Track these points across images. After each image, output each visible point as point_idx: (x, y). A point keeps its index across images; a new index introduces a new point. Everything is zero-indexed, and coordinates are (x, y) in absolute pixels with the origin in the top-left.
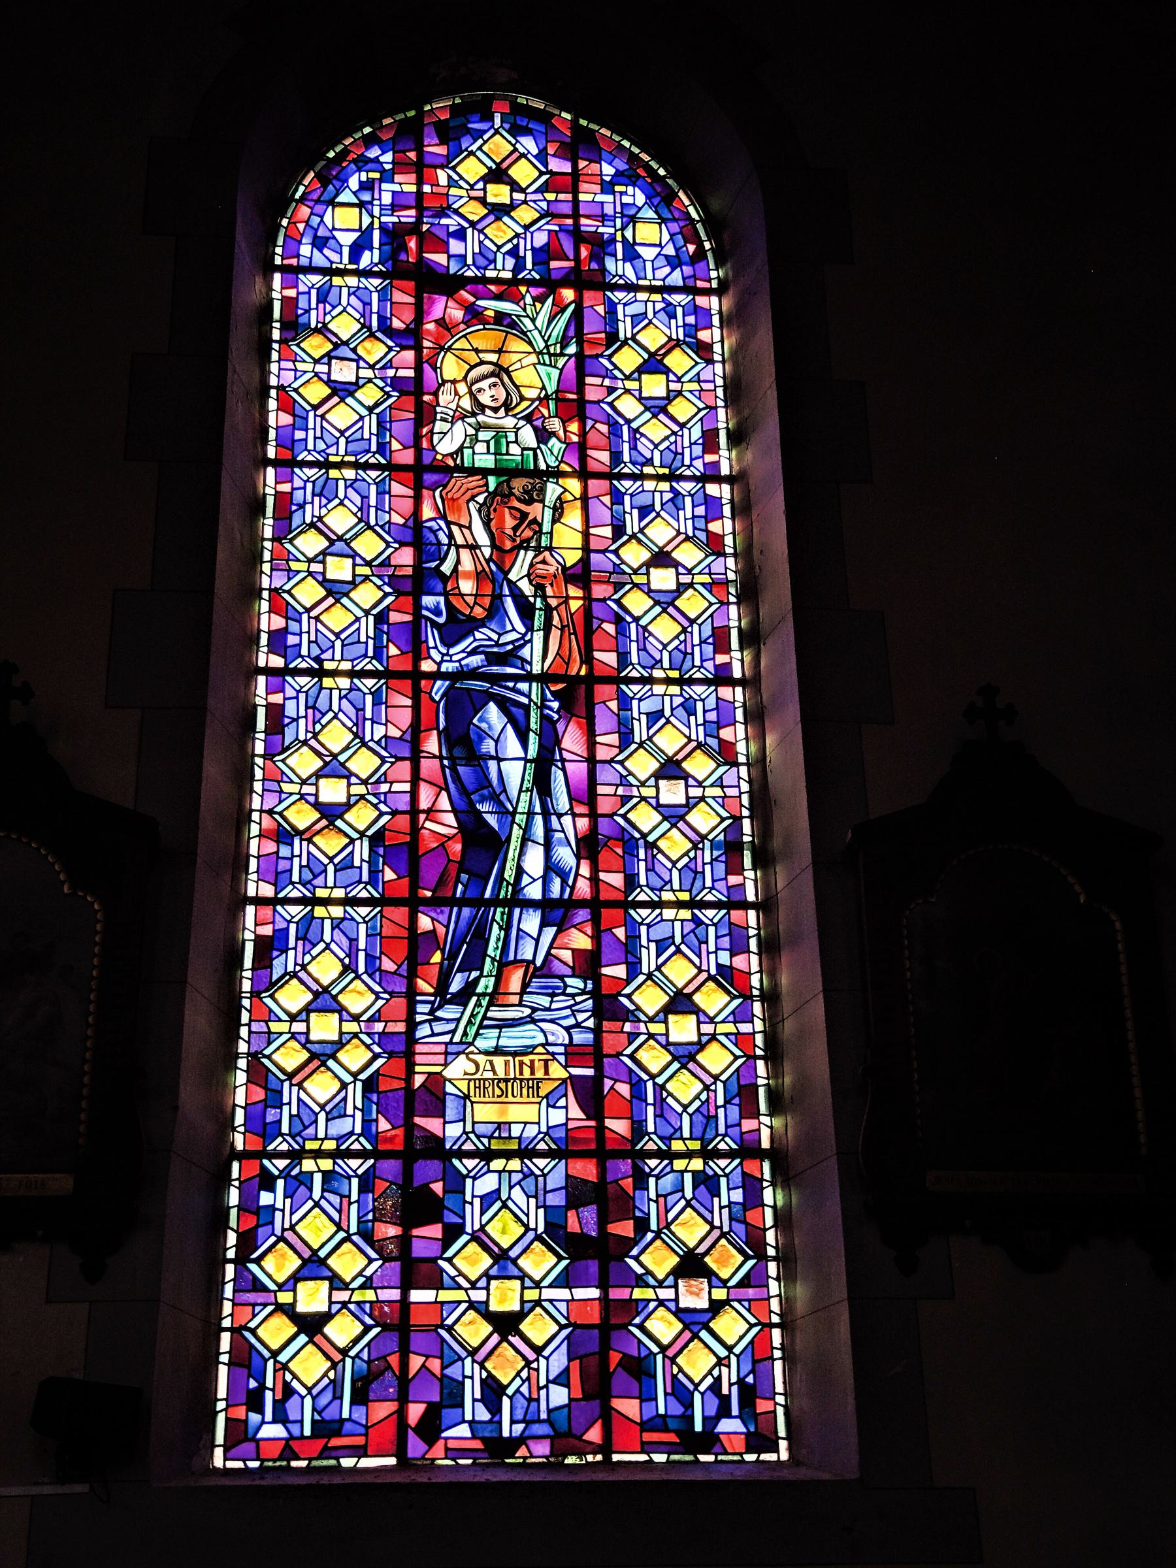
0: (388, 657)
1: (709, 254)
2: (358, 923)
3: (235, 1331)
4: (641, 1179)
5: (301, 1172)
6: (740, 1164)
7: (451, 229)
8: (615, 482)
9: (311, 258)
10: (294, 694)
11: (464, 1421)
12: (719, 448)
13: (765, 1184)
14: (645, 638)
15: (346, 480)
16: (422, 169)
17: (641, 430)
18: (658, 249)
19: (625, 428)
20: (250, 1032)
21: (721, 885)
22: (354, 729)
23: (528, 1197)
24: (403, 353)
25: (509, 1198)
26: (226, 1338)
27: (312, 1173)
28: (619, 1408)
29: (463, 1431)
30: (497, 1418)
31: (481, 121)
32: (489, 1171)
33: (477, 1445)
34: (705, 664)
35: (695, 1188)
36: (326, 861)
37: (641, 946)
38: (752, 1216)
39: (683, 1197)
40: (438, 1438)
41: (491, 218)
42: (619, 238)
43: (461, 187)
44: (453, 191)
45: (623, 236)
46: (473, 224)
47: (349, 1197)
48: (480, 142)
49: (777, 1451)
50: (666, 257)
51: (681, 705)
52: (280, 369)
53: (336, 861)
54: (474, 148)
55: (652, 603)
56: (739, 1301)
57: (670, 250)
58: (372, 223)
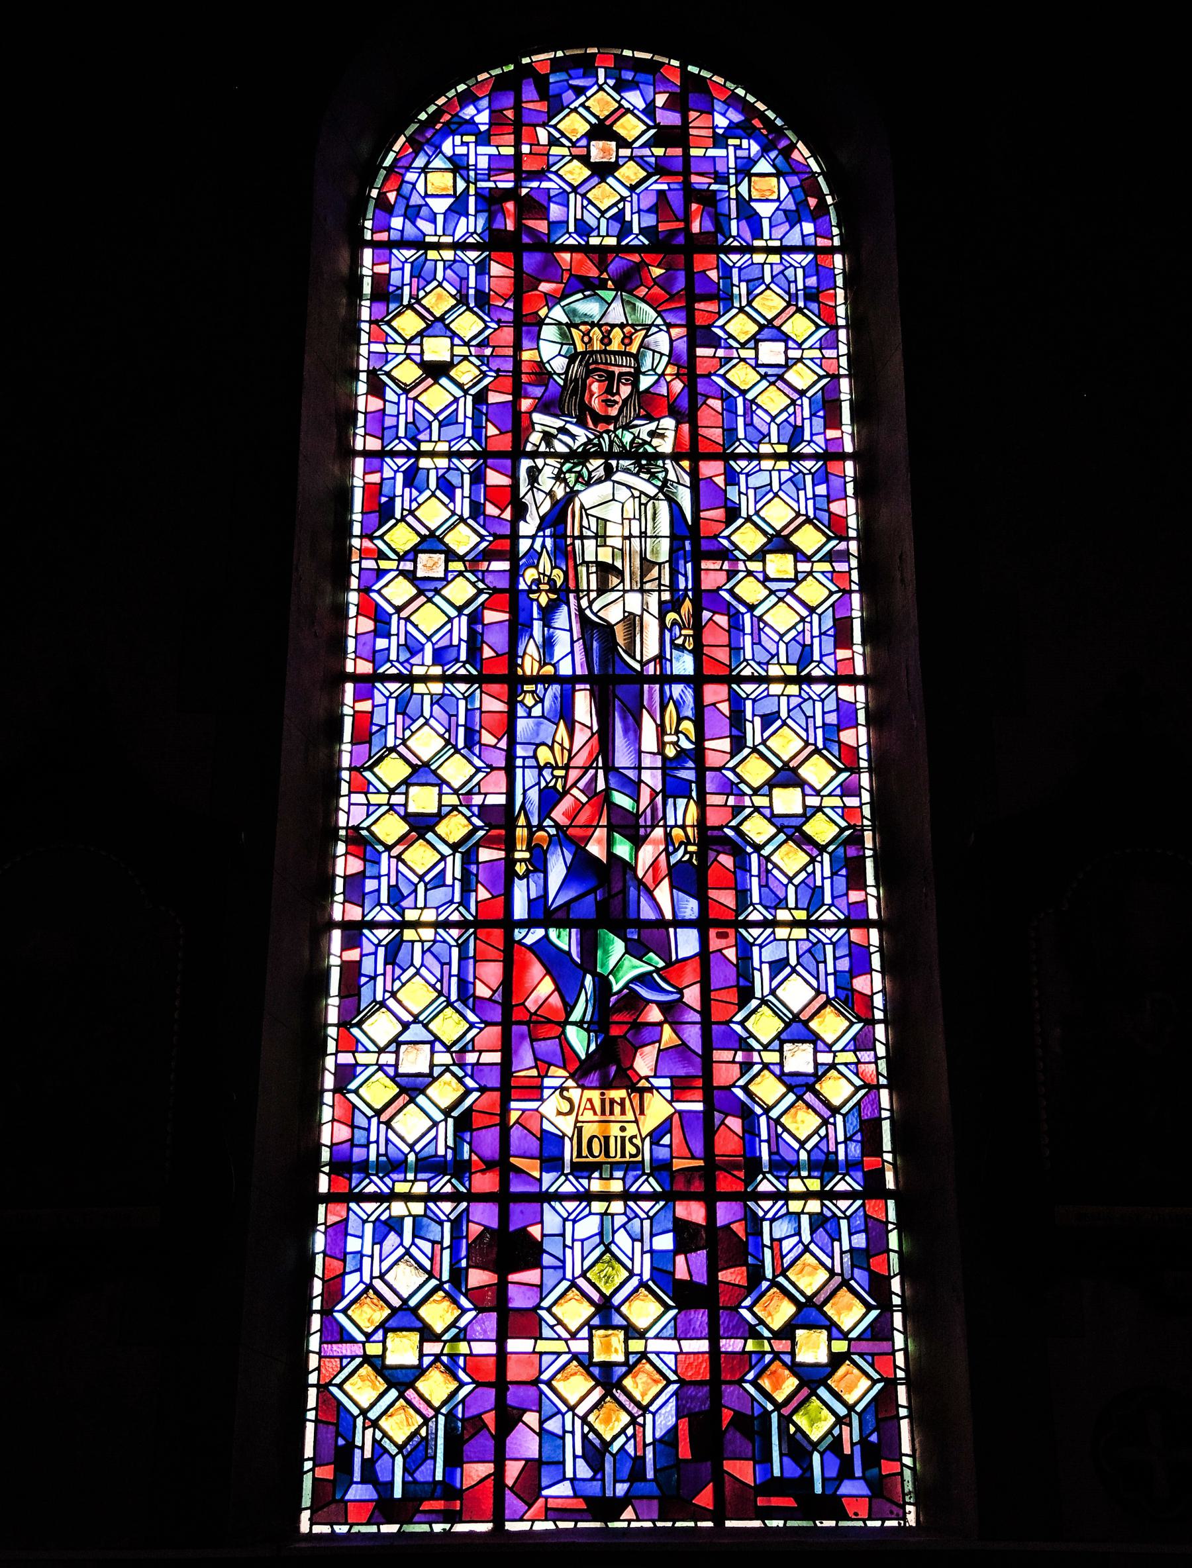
0: (487, 437)
1: (831, 209)
2: (458, 699)
3: (322, 1388)
4: (732, 477)
5: (390, 1217)
6: (863, 1205)
7: (552, 193)
8: (734, 686)
9: (402, 231)
10: (372, 949)
11: (565, 1479)
12: (853, 644)
13: (891, 1227)
14: (760, 630)
15: (444, 261)
16: (519, 128)
17: (758, 401)
18: (777, 204)
19: (740, 401)
20: (361, 569)
21: (842, 903)
22: (438, 986)
23: (634, 1240)
24: (488, 1029)
25: (613, 1242)
26: (312, 1393)
27: (402, 1218)
29: (564, 1489)
30: (599, 1476)
31: (584, 76)
32: (590, 1213)
33: (580, 1504)
34: (824, 659)
35: (812, 1232)
36: (431, 418)
37: (754, 969)
38: (876, 1263)
39: (800, 1241)
40: (539, 1496)
41: (596, 180)
42: (733, 195)
43: (563, 145)
44: (555, 150)
45: (738, 193)
46: (575, 189)
47: (441, 1243)
48: (583, 99)
50: (785, 211)
51: (790, 479)
52: (350, 804)
53: (441, 417)
54: (576, 104)
55: (767, 592)
56: (861, 1355)
57: (790, 204)
58: (467, 188)
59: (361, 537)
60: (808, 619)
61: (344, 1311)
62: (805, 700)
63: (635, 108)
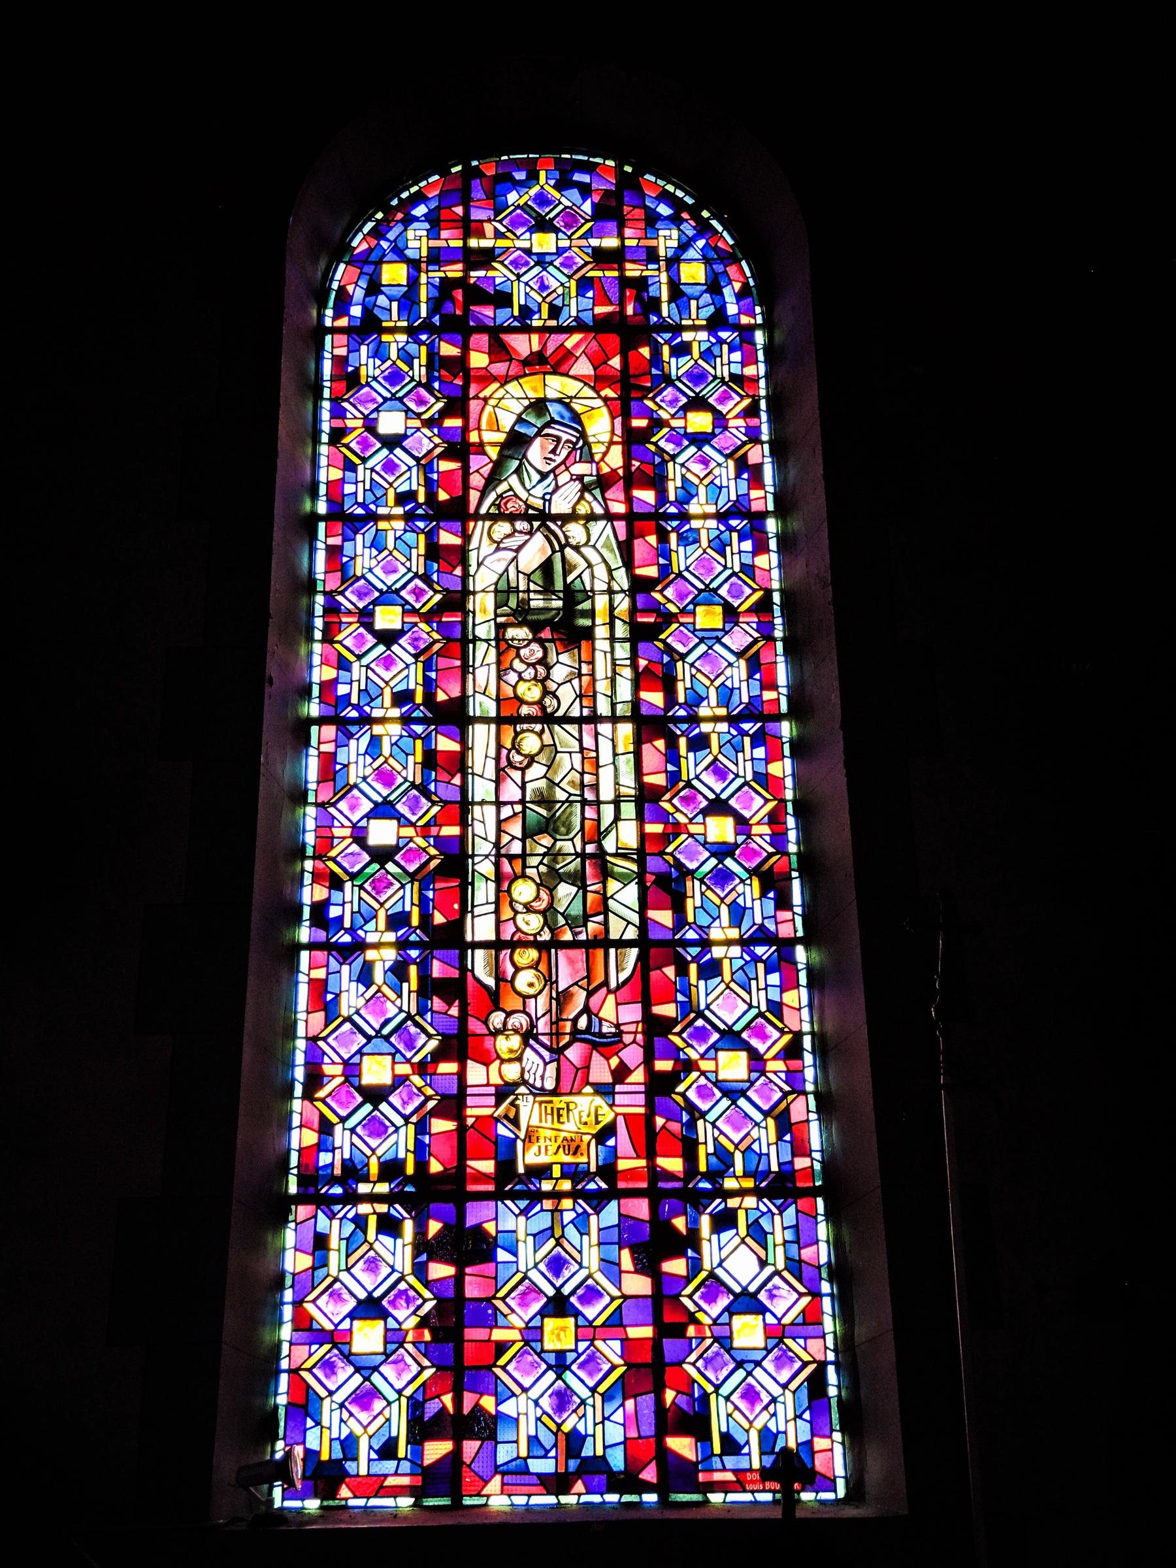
3: (294, 1372)
25: (563, 1236)
28: (653, 917)
43: (508, 238)
49: (835, 1491)
59: (314, 858)
60: (725, 465)
61: (314, 1301)
62: (763, 1214)
63: (574, 204)
